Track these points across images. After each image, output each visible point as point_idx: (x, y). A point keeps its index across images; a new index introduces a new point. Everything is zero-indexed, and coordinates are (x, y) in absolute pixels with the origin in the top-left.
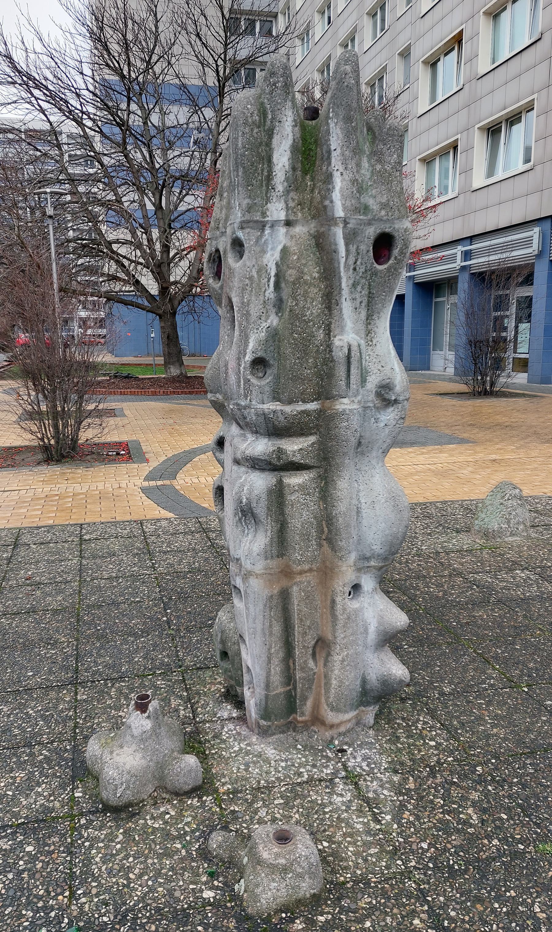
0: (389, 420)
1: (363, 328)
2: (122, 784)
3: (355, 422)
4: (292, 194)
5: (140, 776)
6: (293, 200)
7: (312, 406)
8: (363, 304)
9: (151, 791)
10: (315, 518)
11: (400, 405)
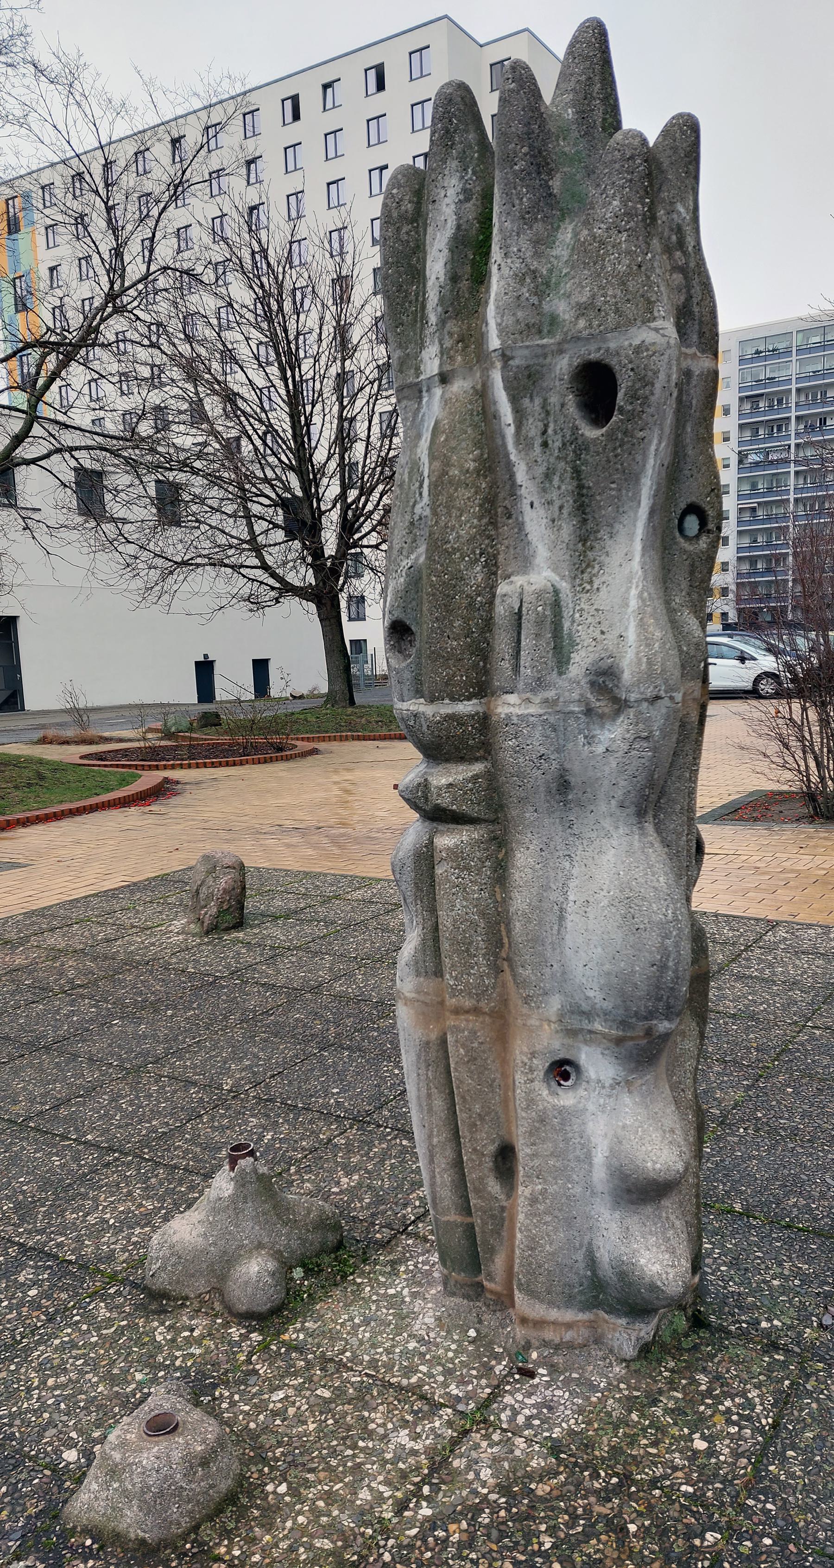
0: (613, 740)
1: (567, 557)
2: (157, 1259)
3: (536, 742)
4: (451, 326)
5: (186, 1260)
6: (451, 334)
7: (466, 708)
8: (565, 511)
9: (202, 1290)
10: (482, 914)
11: (631, 712)
